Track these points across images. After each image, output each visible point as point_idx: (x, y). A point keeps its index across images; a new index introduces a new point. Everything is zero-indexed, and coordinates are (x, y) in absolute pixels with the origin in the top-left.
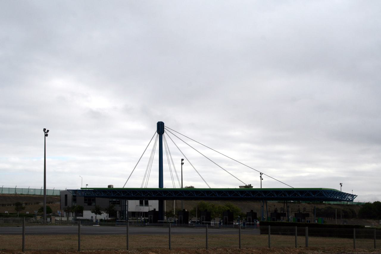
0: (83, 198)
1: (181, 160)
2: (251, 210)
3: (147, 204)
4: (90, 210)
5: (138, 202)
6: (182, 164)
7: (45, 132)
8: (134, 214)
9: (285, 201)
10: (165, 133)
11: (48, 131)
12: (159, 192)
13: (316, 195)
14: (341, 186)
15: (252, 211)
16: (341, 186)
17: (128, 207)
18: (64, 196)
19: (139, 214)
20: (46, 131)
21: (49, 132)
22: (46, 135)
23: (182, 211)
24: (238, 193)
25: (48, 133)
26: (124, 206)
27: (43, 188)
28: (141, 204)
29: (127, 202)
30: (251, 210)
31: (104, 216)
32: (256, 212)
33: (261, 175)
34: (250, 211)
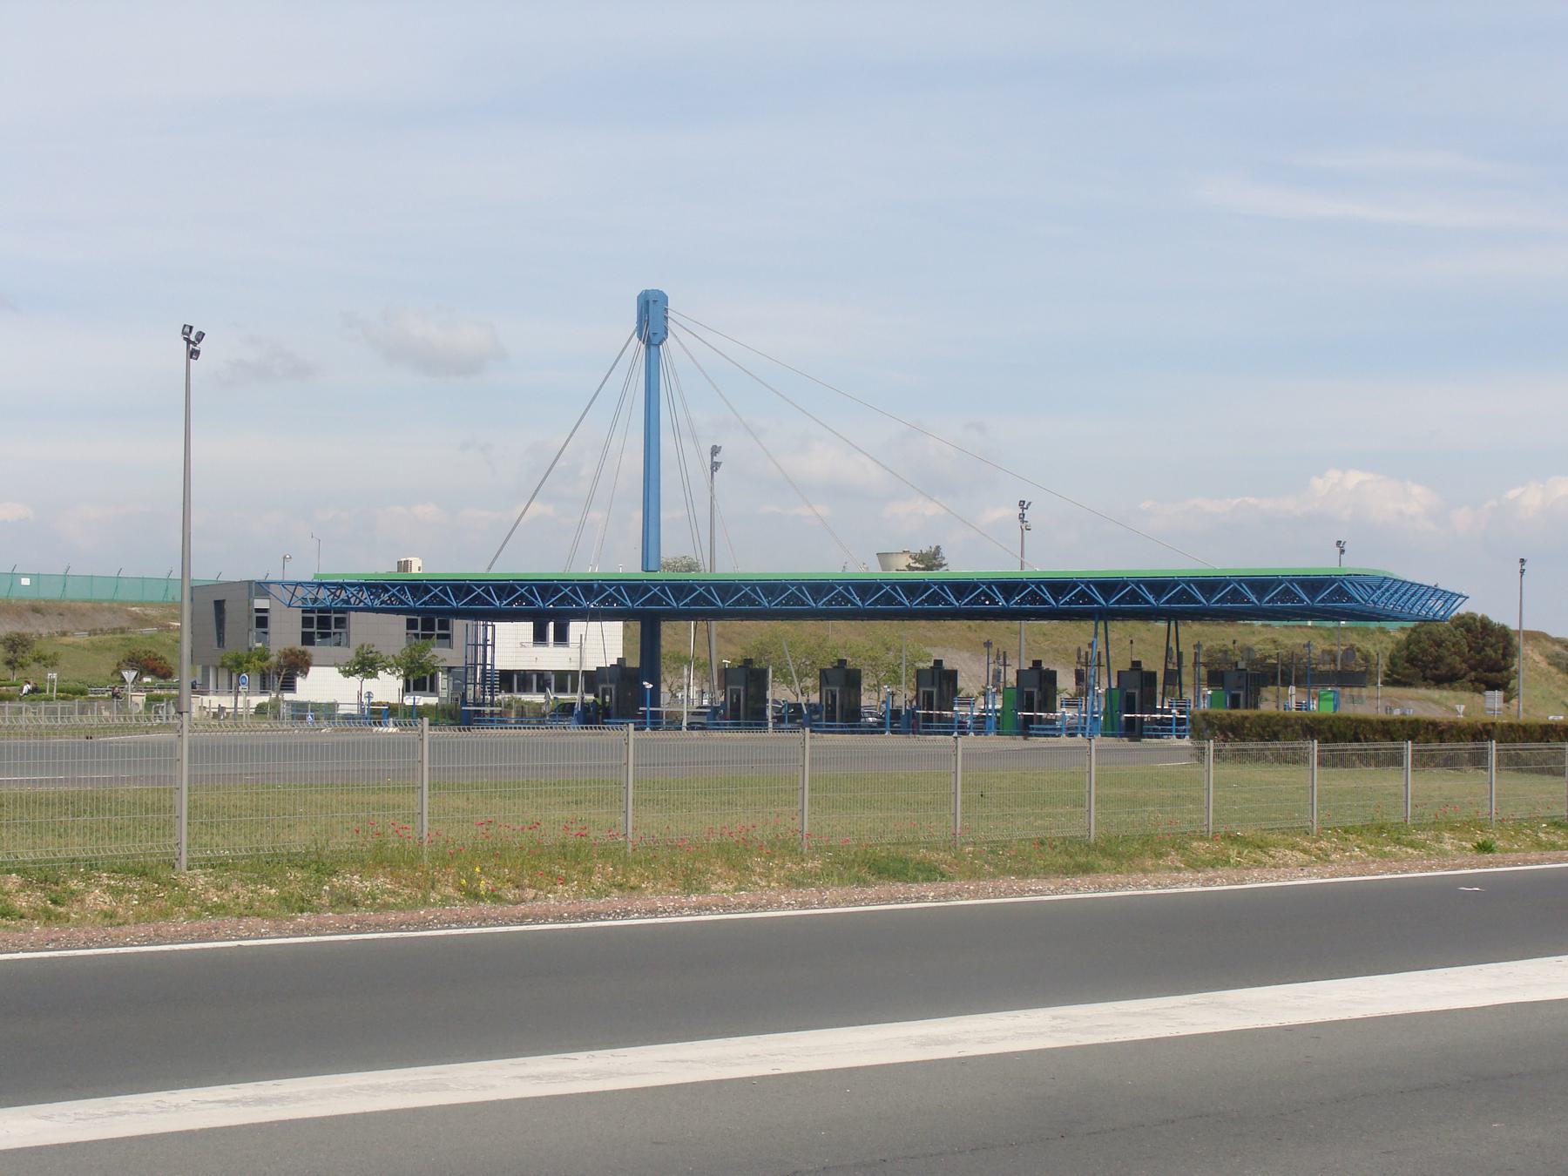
0: (298, 615)
1: (710, 451)
2: (936, 661)
3: (561, 637)
4: (335, 665)
5: (527, 628)
6: (715, 466)
7: (189, 341)
8: (507, 679)
9: (489, 623)
10: (670, 339)
11: (201, 336)
12: (1083, 586)
13: (505, 602)
14: (1342, 551)
15: (1136, 665)
16: (1342, 551)
17: (493, 652)
18: (212, 607)
19: (540, 680)
20: (192, 338)
21: (676, 307)
22: (194, 354)
23: (384, 669)
24: (1241, 586)
25: (199, 347)
26: (480, 649)
27: (177, 575)
28: (540, 637)
29: (490, 628)
30: (936, 661)
31: (387, 687)
32: (1153, 670)
33: (1023, 509)
34: (1129, 666)
